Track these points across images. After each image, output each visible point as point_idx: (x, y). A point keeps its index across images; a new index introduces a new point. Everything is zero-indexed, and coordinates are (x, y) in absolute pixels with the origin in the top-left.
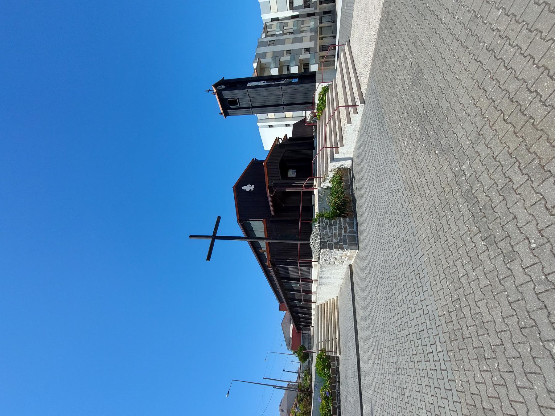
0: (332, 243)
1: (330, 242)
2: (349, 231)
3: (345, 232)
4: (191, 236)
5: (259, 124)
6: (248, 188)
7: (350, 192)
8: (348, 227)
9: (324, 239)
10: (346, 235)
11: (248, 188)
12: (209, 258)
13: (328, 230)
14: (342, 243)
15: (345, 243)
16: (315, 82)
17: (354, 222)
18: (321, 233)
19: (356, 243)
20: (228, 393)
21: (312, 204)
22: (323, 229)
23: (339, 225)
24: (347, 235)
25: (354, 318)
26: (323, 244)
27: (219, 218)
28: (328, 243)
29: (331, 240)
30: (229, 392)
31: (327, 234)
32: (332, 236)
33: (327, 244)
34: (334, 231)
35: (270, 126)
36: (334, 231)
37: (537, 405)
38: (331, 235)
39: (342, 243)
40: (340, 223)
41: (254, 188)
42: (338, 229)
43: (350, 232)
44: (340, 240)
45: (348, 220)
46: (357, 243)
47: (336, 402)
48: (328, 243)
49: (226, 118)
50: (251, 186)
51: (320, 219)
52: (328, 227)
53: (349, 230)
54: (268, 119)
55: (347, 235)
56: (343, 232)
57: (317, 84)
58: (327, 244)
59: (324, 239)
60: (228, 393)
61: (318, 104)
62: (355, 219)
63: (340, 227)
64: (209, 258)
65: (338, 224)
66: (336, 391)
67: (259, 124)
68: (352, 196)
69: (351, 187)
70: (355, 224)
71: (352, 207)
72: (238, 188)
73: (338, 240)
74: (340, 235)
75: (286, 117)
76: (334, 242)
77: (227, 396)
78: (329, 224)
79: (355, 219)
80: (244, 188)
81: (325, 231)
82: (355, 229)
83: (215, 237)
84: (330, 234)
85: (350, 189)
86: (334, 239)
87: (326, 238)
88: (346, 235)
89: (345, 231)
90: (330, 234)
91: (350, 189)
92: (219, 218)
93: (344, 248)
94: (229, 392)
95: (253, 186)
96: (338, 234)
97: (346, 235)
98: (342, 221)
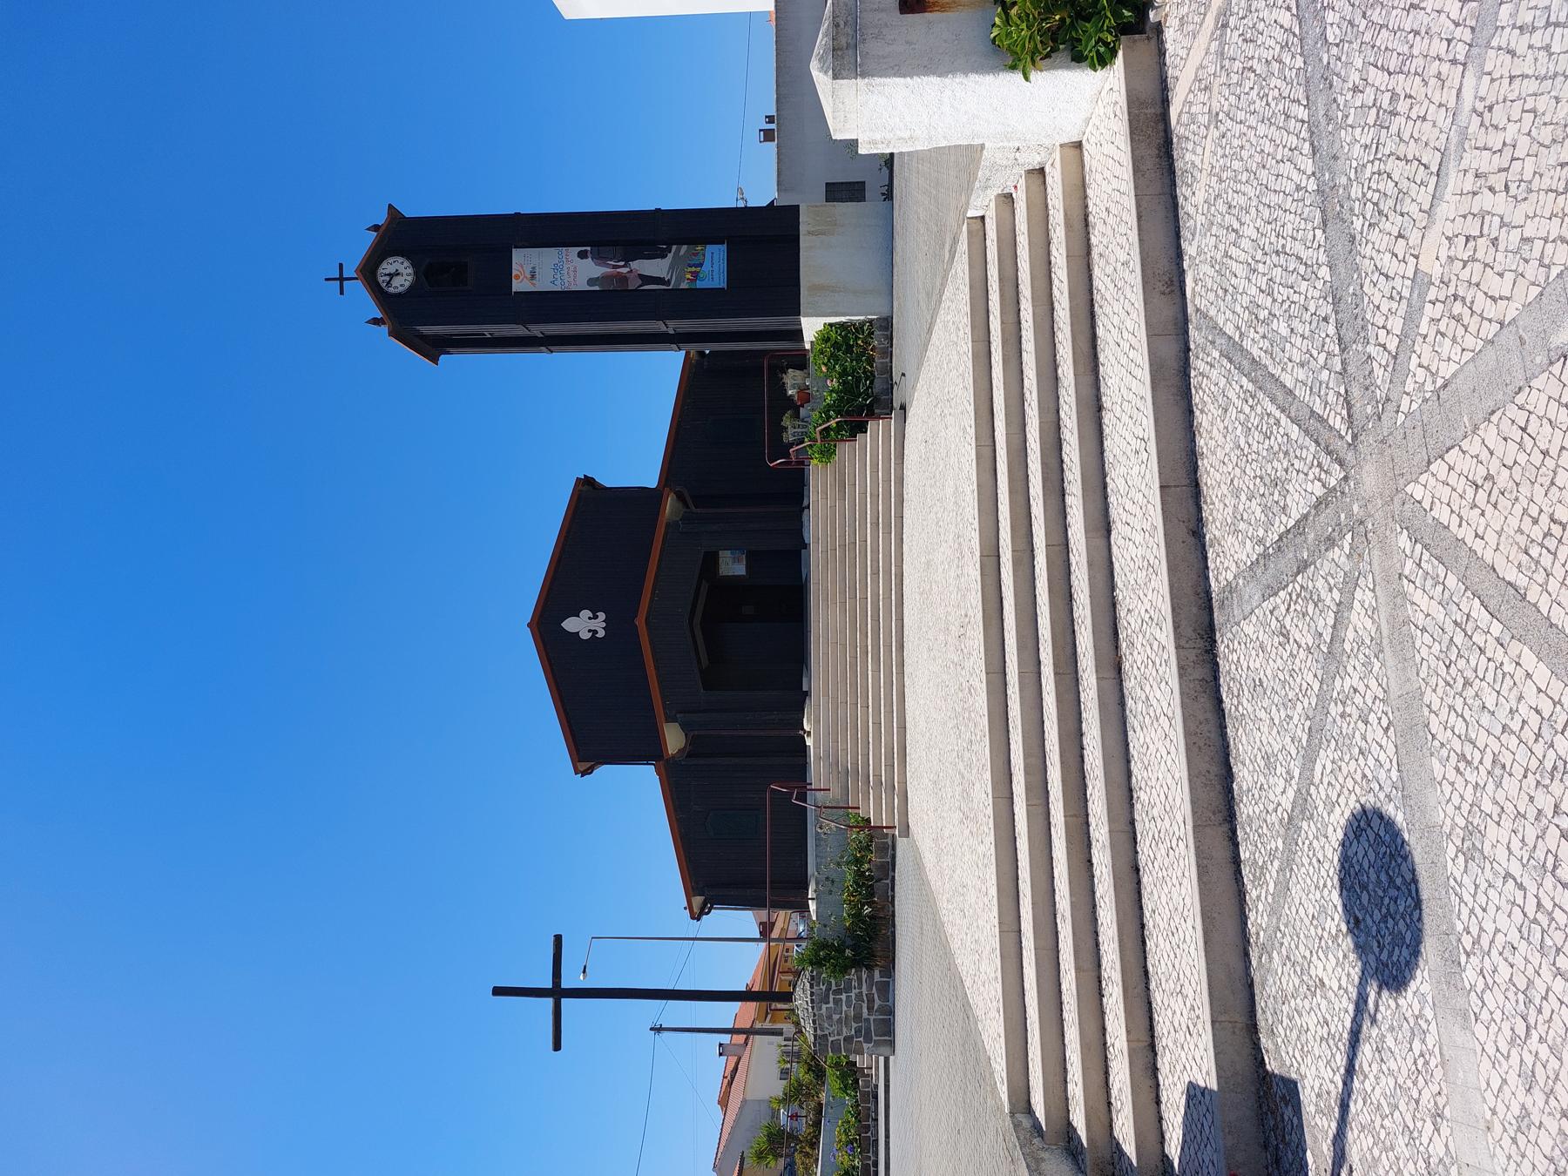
1: (836, 1037)
2: (879, 1008)
3: (870, 1009)
6: (583, 624)
8: (876, 996)
11: (583, 624)
12: (557, 1046)
13: (831, 1005)
14: (861, 1039)
15: (868, 1039)
16: (797, 312)
20: (584, 972)
21: (805, 689)
23: (857, 991)
24: (874, 1017)
27: (558, 940)
28: (830, 1039)
30: (585, 968)
31: (830, 1017)
34: (844, 1008)
36: (844, 1008)
41: (604, 625)
44: (858, 1031)
45: (877, 973)
47: (870, 1154)
48: (830, 1039)
50: (596, 617)
51: (815, 973)
52: (831, 997)
53: (877, 1003)
55: (874, 1017)
56: (865, 1010)
59: (822, 1030)
60: (584, 972)
63: (859, 996)
64: (557, 1046)
66: (869, 1134)
69: (891, 874)
72: (546, 625)
73: (853, 1032)
74: (858, 1017)
76: (845, 1034)
77: (582, 978)
78: (834, 988)
80: (570, 625)
81: (824, 1006)
83: (557, 993)
84: (836, 1017)
87: (826, 1025)
88: (872, 1018)
90: (836, 1017)
92: (558, 940)
94: (585, 968)
95: (602, 616)
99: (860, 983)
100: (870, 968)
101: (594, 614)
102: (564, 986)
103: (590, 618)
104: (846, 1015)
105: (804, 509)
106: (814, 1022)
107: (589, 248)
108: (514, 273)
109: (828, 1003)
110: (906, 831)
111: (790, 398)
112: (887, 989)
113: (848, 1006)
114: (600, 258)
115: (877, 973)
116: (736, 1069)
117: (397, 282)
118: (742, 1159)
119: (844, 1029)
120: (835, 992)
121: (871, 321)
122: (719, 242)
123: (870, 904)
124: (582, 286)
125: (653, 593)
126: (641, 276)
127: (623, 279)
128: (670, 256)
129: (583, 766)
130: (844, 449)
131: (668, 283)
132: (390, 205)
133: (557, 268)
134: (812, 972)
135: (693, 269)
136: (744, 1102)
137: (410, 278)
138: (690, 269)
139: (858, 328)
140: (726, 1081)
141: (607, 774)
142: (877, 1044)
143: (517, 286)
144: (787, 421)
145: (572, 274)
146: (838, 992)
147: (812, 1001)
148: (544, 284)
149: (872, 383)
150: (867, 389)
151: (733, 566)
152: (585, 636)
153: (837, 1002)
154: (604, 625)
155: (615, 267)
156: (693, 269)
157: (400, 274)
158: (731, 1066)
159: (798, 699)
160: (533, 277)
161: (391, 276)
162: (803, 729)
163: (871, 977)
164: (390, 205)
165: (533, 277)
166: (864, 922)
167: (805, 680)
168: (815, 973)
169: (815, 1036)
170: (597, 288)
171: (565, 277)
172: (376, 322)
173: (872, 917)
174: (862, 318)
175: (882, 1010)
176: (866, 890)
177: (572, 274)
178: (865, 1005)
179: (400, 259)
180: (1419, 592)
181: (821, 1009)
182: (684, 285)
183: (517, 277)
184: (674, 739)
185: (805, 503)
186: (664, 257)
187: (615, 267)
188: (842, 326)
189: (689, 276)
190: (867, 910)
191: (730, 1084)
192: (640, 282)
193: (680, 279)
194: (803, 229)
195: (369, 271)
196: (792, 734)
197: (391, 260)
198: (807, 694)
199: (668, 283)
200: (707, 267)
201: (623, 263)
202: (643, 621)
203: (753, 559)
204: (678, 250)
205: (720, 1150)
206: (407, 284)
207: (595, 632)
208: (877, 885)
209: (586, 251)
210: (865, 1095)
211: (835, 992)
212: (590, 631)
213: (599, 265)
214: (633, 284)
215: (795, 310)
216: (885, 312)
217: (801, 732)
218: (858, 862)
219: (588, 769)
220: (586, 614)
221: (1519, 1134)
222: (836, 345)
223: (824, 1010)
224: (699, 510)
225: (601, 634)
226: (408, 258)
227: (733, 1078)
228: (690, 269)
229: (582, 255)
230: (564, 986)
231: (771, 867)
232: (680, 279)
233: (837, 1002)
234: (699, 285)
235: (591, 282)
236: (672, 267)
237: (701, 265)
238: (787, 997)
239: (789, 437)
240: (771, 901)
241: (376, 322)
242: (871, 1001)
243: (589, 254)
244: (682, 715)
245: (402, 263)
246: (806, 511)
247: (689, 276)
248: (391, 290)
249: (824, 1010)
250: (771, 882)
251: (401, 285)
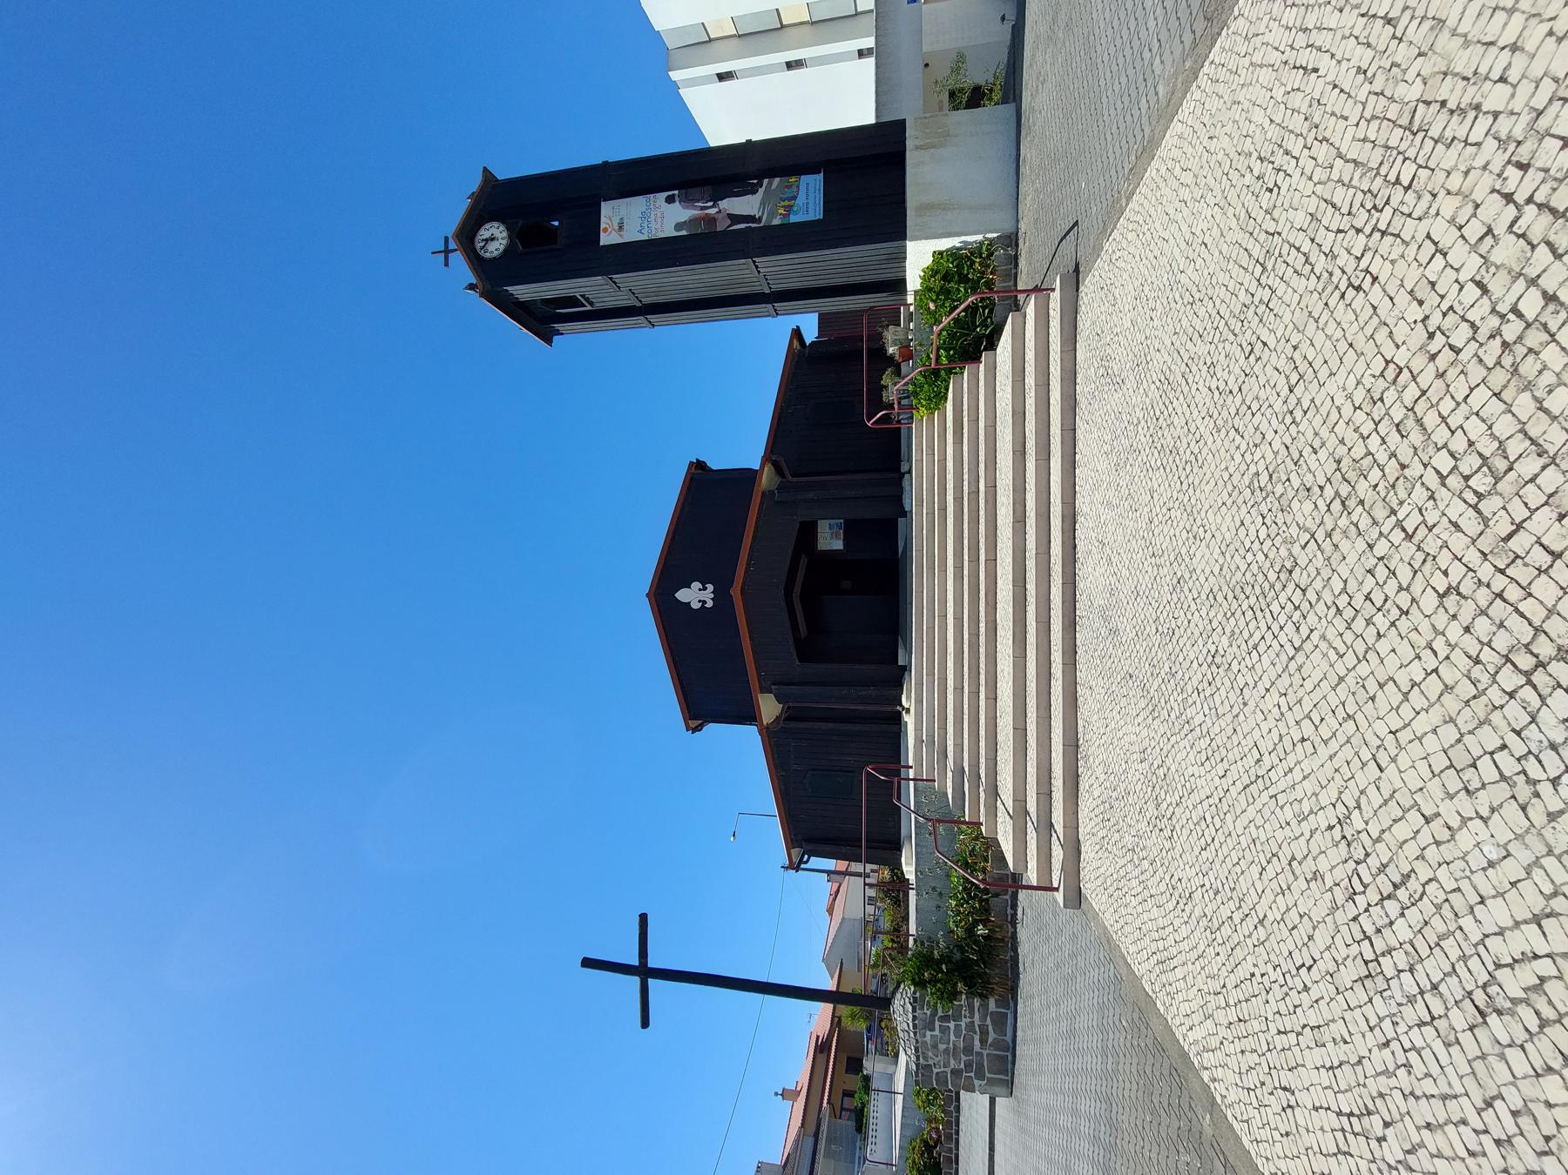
0: (945, 1069)
1: (942, 1069)
3: (983, 1041)
4: (588, 963)
5: (675, 75)
6: (695, 595)
7: (1009, 908)
8: (990, 1028)
9: (925, 1058)
10: (985, 1052)
11: (695, 595)
12: (645, 1023)
13: (937, 1032)
14: (972, 1074)
15: (980, 1076)
17: (1009, 1015)
18: (919, 1040)
19: (1006, 1078)
21: (901, 663)
22: (925, 1029)
25: (989, 1154)
26: (923, 1075)
27: (643, 919)
28: (935, 1071)
29: (944, 1064)
31: (935, 1046)
32: (946, 1051)
33: (935, 1073)
34: (952, 1037)
35: (722, 77)
36: (952, 1037)
37: (1481, 300)
38: (945, 1050)
39: (972, 1074)
40: (972, 1016)
41: (712, 596)
42: (964, 1032)
43: (996, 1045)
44: (968, 1065)
45: (992, 1003)
46: (1009, 1078)
48: (935, 1071)
49: (551, 346)
50: (705, 589)
51: (918, 995)
52: (937, 1024)
53: (992, 1036)
54: (710, 40)
56: (977, 1043)
57: (911, 246)
58: (935, 1073)
59: (925, 1058)
61: (916, 292)
62: (1012, 1005)
63: (970, 1026)
64: (645, 1023)
65: (965, 1017)
67: (675, 75)
68: (1011, 923)
70: (1010, 1016)
71: (1009, 965)
73: (962, 1066)
74: (968, 1050)
75: (783, 26)
77: (732, 839)
78: (940, 1013)
79: (1012, 1005)
80: (683, 595)
81: (928, 1033)
82: (1009, 1038)
83: (644, 972)
84: (942, 1047)
85: (1010, 893)
86: (952, 1062)
87: (930, 1054)
88: (985, 1052)
89: (981, 1041)
90: (942, 1047)
91: (1010, 893)
92: (643, 919)
93: (977, 1088)
95: (710, 587)
96: (964, 1048)
97: (983, 1051)
98: (976, 1009)
99: (972, 1013)
100: (983, 997)
101: (703, 586)
102: (651, 965)
103: (700, 590)
104: (954, 1045)
105: (903, 474)
106: (917, 1050)
107: (676, 192)
108: (603, 226)
109: (933, 1029)
111: (891, 358)
112: (1006, 1020)
113: (957, 1036)
114: (687, 200)
115: (992, 1003)
116: (838, 891)
118: (842, 963)
119: (952, 1062)
120: (943, 1019)
121: (991, 241)
122: (811, 169)
123: (985, 922)
124: (669, 232)
125: (748, 564)
126: (730, 216)
127: (711, 220)
128: (761, 191)
129: (693, 724)
130: (964, 382)
131: (760, 220)
132: (485, 168)
133: (644, 216)
134: (915, 993)
135: (786, 203)
136: (843, 919)
137: (504, 242)
138: (782, 204)
139: (976, 251)
140: (832, 897)
141: (715, 731)
142: (991, 1082)
143: (606, 239)
144: (886, 379)
145: (659, 220)
146: (945, 1018)
147: (915, 1026)
148: (632, 235)
149: (991, 311)
150: (986, 319)
151: (830, 539)
152: (696, 605)
153: (944, 1030)
154: (712, 596)
155: (703, 208)
156: (786, 203)
157: (495, 238)
158: (835, 888)
159: (896, 677)
160: (621, 228)
161: (487, 240)
162: (901, 705)
163: (984, 1006)
164: (485, 168)
165: (621, 228)
166: (976, 942)
167: (901, 652)
168: (918, 995)
169: (917, 1065)
170: (684, 233)
171: (653, 225)
172: (472, 287)
173: (986, 937)
174: (979, 237)
175: (997, 1045)
176: (980, 903)
177: (659, 220)
178: (977, 1037)
179: (496, 224)
181: (925, 1036)
182: (776, 221)
183: (605, 230)
184: (769, 708)
185: (904, 468)
186: (754, 192)
187: (703, 208)
188: (953, 254)
189: (782, 211)
190: (981, 930)
191: (834, 900)
192: (729, 222)
193: (772, 215)
194: (909, 144)
195: (467, 235)
197: (487, 226)
198: (905, 669)
199: (760, 220)
200: (801, 200)
201: (710, 204)
202: (739, 591)
203: (852, 530)
204: (770, 184)
205: (828, 948)
206: (502, 248)
207: (704, 602)
208: (993, 901)
209: (674, 195)
211: (943, 1019)
212: (700, 601)
213: (687, 208)
215: (898, 232)
216: (1008, 227)
217: (899, 708)
219: (699, 726)
220: (696, 585)
221: (1290, 906)
222: (946, 277)
223: (928, 1038)
224: (795, 479)
225: (710, 604)
226: (503, 223)
227: (836, 896)
228: (782, 204)
229: (670, 200)
230: (651, 965)
231: (867, 825)
232: (772, 215)
233: (944, 1030)
234: (793, 219)
235: (678, 226)
236: (763, 203)
237: (795, 198)
238: (886, 1003)
240: (866, 856)
242: (984, 1033)
243: (677, 198)
244: (777, 687)
245: (498, 228)
246: (907, 476)
247: (782, 211)
248: (488, 255)
249: (928, 1038)
250: (867, 841)
251: (496, 250)
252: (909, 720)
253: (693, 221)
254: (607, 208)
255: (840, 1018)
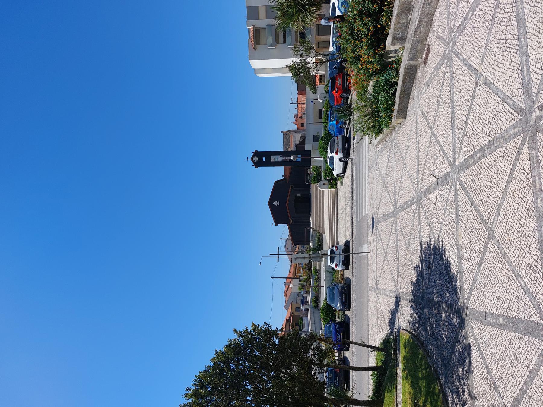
6: (276, 203)
11: (276, 203)
72: (270, 204)
80: (274, 203)
83: (278, 254)
95: (279, 202)
110: (324, 233)
114: (283, 157)
117: (256, 160)
127: (287, 160)
136: (291, 292)
143: (272, 161)
148: (276, 160)
152: (276, 205)
157: (256, 159)
172: (253, 166)
180: (505, 151)
191: (287, 291)
195: (252, 159)
196: (290, 217)
210: (319, 274)
214: (288, 161)
218: (318, 238)
220: (276, 202)
225: (279, 205)
229: (281, 157)
234: (297, 161)
235: (282, 160)
239: (308, 179)
241: (253, 166)
252: (311, 222)
253: (284, 160)
254: (272, 156)
255: (293, 312)
